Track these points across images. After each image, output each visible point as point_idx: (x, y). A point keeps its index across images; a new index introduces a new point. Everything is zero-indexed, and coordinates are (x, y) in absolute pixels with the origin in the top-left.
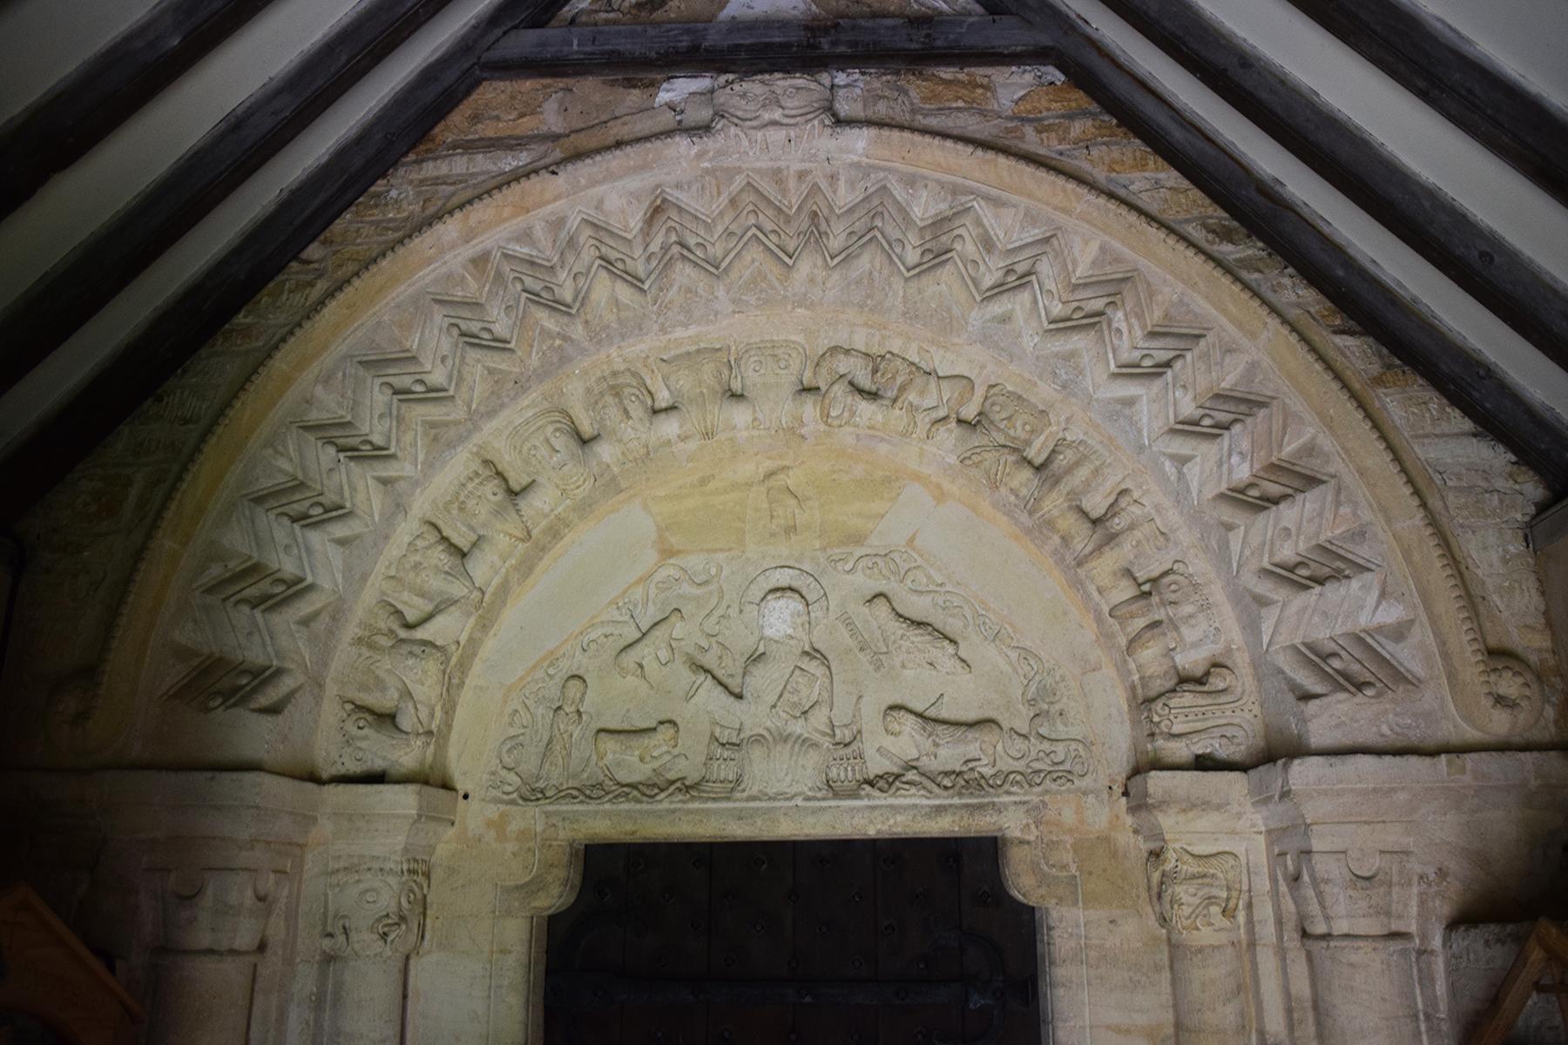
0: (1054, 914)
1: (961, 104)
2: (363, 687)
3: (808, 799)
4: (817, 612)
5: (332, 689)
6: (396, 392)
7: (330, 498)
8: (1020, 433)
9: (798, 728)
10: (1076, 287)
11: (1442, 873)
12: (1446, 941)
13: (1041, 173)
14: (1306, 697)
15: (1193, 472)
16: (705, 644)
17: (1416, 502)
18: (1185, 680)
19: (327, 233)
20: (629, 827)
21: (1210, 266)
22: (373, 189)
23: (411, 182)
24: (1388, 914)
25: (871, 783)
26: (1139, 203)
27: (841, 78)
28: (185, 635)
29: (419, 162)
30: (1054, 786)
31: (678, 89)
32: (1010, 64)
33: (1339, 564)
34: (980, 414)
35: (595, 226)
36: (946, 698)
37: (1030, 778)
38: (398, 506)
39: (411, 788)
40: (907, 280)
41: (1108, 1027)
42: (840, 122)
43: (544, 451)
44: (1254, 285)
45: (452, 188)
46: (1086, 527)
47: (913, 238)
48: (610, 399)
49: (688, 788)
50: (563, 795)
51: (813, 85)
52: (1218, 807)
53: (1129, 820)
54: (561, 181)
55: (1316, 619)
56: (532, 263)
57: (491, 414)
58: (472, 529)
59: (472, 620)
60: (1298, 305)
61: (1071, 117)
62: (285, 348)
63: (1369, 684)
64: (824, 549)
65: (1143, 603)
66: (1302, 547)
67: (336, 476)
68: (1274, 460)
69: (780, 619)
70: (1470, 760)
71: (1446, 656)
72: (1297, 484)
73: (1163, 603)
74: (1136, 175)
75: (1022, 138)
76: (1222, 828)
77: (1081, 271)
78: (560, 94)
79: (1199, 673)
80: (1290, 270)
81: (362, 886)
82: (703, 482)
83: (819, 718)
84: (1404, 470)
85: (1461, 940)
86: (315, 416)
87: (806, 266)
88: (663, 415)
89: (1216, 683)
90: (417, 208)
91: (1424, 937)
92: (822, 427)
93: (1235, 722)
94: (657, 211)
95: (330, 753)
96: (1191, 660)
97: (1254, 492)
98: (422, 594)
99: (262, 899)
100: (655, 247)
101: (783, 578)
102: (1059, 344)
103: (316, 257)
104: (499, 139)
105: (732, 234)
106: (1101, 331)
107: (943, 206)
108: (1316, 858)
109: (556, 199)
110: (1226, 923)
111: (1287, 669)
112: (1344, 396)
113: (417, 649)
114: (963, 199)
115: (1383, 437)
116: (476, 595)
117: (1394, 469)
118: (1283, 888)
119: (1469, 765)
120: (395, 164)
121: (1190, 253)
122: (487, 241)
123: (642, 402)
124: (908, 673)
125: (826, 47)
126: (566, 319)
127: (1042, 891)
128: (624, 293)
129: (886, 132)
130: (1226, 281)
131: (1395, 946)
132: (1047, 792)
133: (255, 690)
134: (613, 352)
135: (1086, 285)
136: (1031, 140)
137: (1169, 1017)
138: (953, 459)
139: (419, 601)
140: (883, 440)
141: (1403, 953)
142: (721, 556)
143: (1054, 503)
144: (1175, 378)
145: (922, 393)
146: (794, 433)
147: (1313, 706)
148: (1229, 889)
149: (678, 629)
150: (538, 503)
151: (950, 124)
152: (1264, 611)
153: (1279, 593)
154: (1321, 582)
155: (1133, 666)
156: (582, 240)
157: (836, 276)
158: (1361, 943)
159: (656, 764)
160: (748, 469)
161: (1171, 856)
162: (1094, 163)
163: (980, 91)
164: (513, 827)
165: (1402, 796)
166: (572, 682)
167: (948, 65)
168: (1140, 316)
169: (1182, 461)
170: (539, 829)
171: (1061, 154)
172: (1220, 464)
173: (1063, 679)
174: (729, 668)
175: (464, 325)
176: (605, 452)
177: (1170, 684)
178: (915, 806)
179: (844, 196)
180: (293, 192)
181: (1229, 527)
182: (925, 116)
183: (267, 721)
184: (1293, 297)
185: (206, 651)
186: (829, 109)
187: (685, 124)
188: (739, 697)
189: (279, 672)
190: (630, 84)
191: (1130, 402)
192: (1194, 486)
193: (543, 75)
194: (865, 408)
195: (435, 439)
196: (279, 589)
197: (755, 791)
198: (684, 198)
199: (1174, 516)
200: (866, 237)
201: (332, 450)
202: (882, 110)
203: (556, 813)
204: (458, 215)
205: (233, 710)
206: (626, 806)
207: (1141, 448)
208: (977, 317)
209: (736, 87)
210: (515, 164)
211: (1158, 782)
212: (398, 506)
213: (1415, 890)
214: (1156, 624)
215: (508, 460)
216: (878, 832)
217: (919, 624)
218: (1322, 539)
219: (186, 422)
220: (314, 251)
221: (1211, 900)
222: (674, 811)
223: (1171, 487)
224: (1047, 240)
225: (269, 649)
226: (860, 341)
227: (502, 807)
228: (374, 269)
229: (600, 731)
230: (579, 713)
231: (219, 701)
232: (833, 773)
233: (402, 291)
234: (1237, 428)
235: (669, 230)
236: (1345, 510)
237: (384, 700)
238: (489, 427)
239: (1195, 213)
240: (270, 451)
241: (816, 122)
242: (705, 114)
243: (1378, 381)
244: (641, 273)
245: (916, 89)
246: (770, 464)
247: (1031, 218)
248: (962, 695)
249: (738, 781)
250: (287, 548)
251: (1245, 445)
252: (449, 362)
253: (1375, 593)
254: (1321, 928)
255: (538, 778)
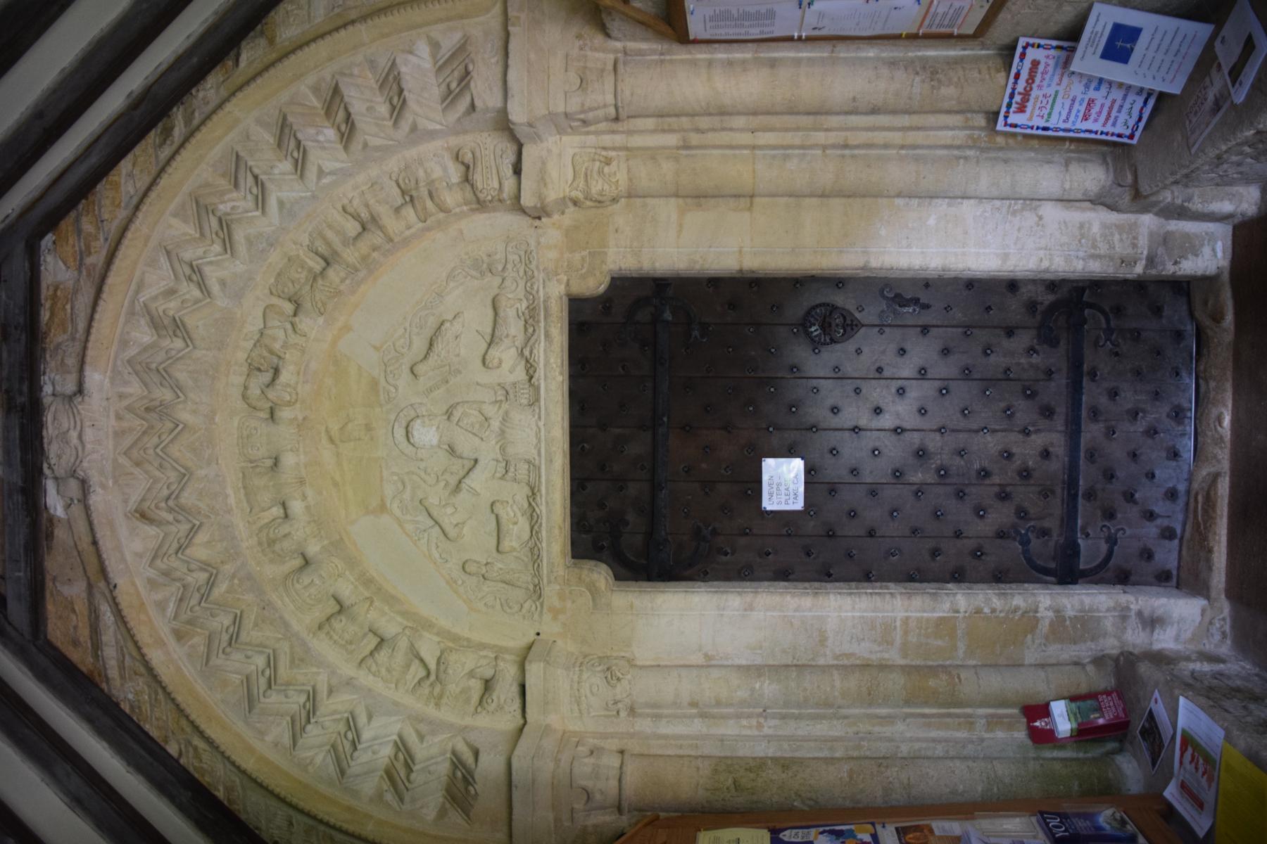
0: (612, 266)
1: (68, 307)
2: (468, 701)
3: (540, 418)
4: (423, 411)
5: (468, 721)
6: (270, 687)
7: (342, 727)
8: (304, 275)
9: (495, 424)
10: (202, 234)
11: (579, 37)
12: (617, 39)
13: (120, 254)
14: (473, 107)
15: (329, 165)
16: (442, 484)
17: (350, 28)
18: (467, 179)
19: (159, 741)
20: (556, 531)
21: (189, 146)
22: (127, 711)
23: (122, 685)
24: (603, 70)
25: (531, 378)
26: (144, 188)
27: (48, 389)
28: (430, 813)
29: (108, 680)
30: (534, 263)
31: (55, 502)
32: (39, 272)
33: (391, 78)
34: (290, 300)
35: (154, 558)
36: (480, 329)
37: (530, 277)
38: (348, 684)
39: (527, 667)
40: (195, 348)
41: (678, 237)
42: (80, 390)
43: (312, 590)
44: (203, 116)
45: (127, 657)
46: (367, 236)
47: (166, 343)
48: (277, 547)
49: (533, 492)
50: (537, 573)
51: (53, 409)
52: (544, 163)
53: (556, 217)
54: (121, 581)
55: (426, 95)
56: (181, 600)
57: (286, 625)
58: (365, 635)
59: (426, 634)
60: (218, 88)
61: (79, 232)
62: (239, 761)
63: (466, 67)
64: (381, 406)
65: (416, 202)
66: (380, 99)
67: (327, 724)
68: (322, 112)
69: (426, 435)
70: (511, 13)
71: (449, 19)
72: (338, 100)
73: (417, 188)
74: (123, 188)
75: (94, 266)
76: (558, 162)
77: (191, 230)
78: (58, 584)
79: (462, 168)
80: (194, 91)
81: (589, 694)
82: (336, 484)
83: (490, 410)
84: (330, 33)
85: (615, 33)
86: (287, 740)
87: (184, 416)
88: (289, 512)
89: (468, 158)
90: (141, 681)
91: (616, 51)
92: (298, 405)
93: (491, 151)
94: (143, 516)
95: (507, 721)
96: (455, 173)
97: (343, 127)
98: (408, 666)
99: (592, 752)
100: (170, 518)
101: (400, 433)
102: (241, 248)
103: (177, 747)
104: (91, 626)
105: (161, 465)
106: (232, 220)
107: (143, 322)
108: (569, 110)
109: (134, 584)
110: (614, 163)
111: (457, 115)
112: (279, 66)
113: (442, 667)
114: (138, 308)
115: (307, 43)
116: (407, 631)
117: (328, 39)
118: (592, 128)
119: (515, 14)
120: (109, 698)
121: (178, 158)
122: (165, 631)
123: (279, 525)
124: (463, 352)
125: (23, 399)
126: (220, 577)
127: (598, 274)
128: (201, 537)
129: (88, 359)
130: (199, 136)
131: (621, 67)
132: (537, 267)
133: (464, 766)
134: (245, 545)
135: (201, 228)
136: (96, 259)
137: (673, 200)
138: (321, 320)
139: (413, 669)
140: (307, 366)
141: (625, 63)
142: (385, 473)
143: (350, 255)
144: (265, 173)
145: (275, 339)
146: (302, 425)
147: (478, 103)
148: (594, 160)
149: (433, 501)
150: (347, 593)
151: (83, 314)
152: (420, 127)
153: (408, 118)
154: (401, 91)
155: (457, 210)
156: (163, 566)
157: (191, 395)
158: (619, 89)
159: (519, 514)
160: (327, 454)
161: (574, 194)
162: (113, 217)
163: (59, 293)
164: (556, 603)
165: (532, 56)
166: (467, 569)
167: (38, 314)
168: (223, 193)
169: (321, 173)
170: (558, 587)
171: (106, 239)
172: (324, 148)
173: (467, 254)
174: (458, 467)
175: (224, 644)
176: (313, 549)
177: (468, 188)
178: (545, 350)
179: (135, 388)
180: (129, 764)
181: (365, 145)
182: (77, 331)
183: (483, 758)
184: (213, 91)
185: (441, 800)
186: (70, 398)
187: (80, 497)
188: (476, 461)
189: (454, 753)
190: (50, 536)
191: (281, 204)
192: (338, 165)
193: (43, 597)
194: (285, 377)
195: (302, 660)
196: (401, 756)
197: (535, 452)
198: (134, 499)
199: (361, 178)
200: (164, 375)
201: (309, 727)
202: (71, 361)
203: (548, 576)
204: (145, 650)
205: (476, 777)
206: (544, 533)
207: (314, 197)
208: (221, 302)
209: (53, 462)
210: (109, 614)
211: (527, 200)
212: (348, 684)
213: (589, 53)
214: (431, 195)
215: (318, 614)
216: (561, 373)
217: (431, 345)
218: (376, 86)
219: (291, 824)
220: (173, 749)
221: (600, 172)
222: (547, 503)
223: (337, 181)
224: (168, 253)
225: (439, 759)
226: (238, 380)
227: (545, 610)
228: (183, 706)
229: (498, 550)
230: (487, 564)
231: (471, 788)
232: (525, 402)
233: (200, 687)
234: (300, 136)
235: (157, 507)
236: (356, 71)
237: (476, 686)
238: (295, 626)
239: (151, 151)
240: (310, 768)
241: (80, 407)
242: (73, 485)
243: (271, 41)
244: (188, 526)
245: (56, 337)
246: (325, 441)
247: (153, 263)
248: (476, 319)
249: (529, 462)
250: (374, 753)
251: (312, 131)
252: (250, 653)
253: (410, 57)
254: (612, 111)
255: (527, 589)
